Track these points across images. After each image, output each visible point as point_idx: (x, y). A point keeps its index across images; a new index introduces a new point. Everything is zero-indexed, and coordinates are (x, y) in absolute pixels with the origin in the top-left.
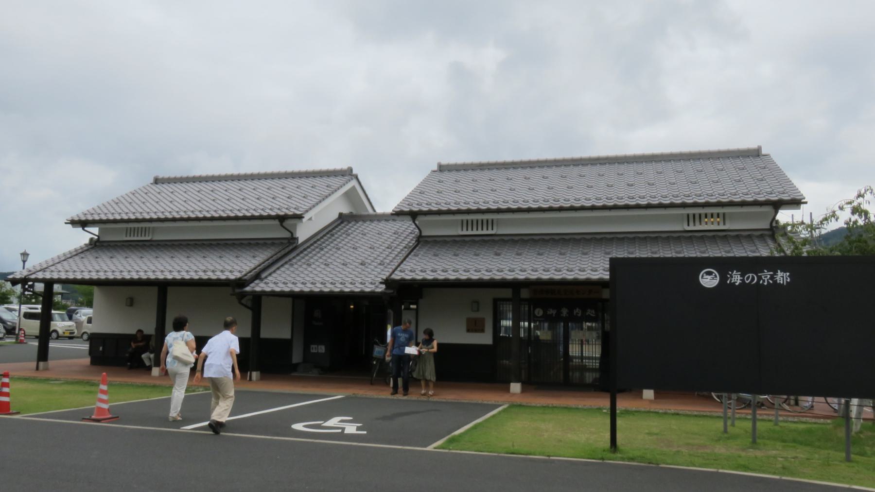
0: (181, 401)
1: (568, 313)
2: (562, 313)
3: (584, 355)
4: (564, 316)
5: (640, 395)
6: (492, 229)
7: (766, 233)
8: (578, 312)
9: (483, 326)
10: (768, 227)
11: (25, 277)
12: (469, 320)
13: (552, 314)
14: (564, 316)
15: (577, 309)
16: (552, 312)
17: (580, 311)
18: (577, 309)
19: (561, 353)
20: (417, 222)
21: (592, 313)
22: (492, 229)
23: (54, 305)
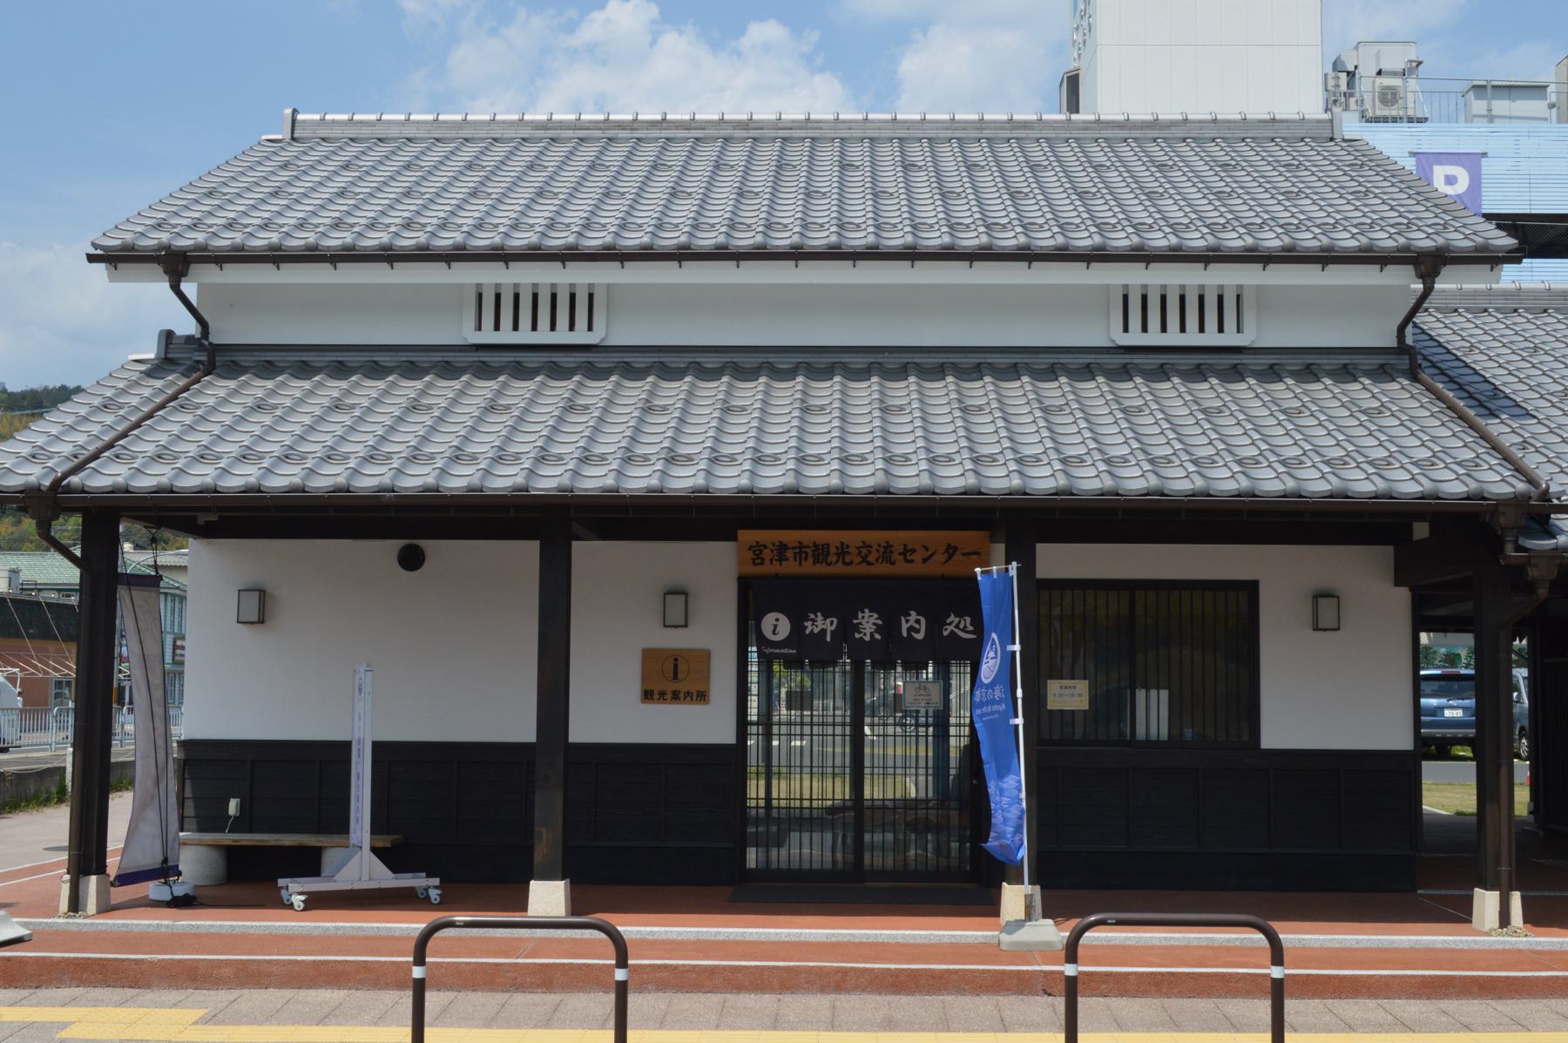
0: (609, 921)
1: (879, 629)
2: (857, 628)
3: (867, 795)
4: (867, 638)
5: (1461, 913)
6: (590, 328)
7: (1392, 360)
8: (914, 624)
9: (705, 675)
10: (1392, 342)
11: (57, 483)
12: (649, 656)
13: (823, 631)
14: (867, 638)
15: (913, 615)
16: (822, 625)
17: (923, 620)
18: (913, 615)
19: (951, 777)
20: (189, 288)
21: (964, 630)
22: (590, 328)
23: (1560, 565)
